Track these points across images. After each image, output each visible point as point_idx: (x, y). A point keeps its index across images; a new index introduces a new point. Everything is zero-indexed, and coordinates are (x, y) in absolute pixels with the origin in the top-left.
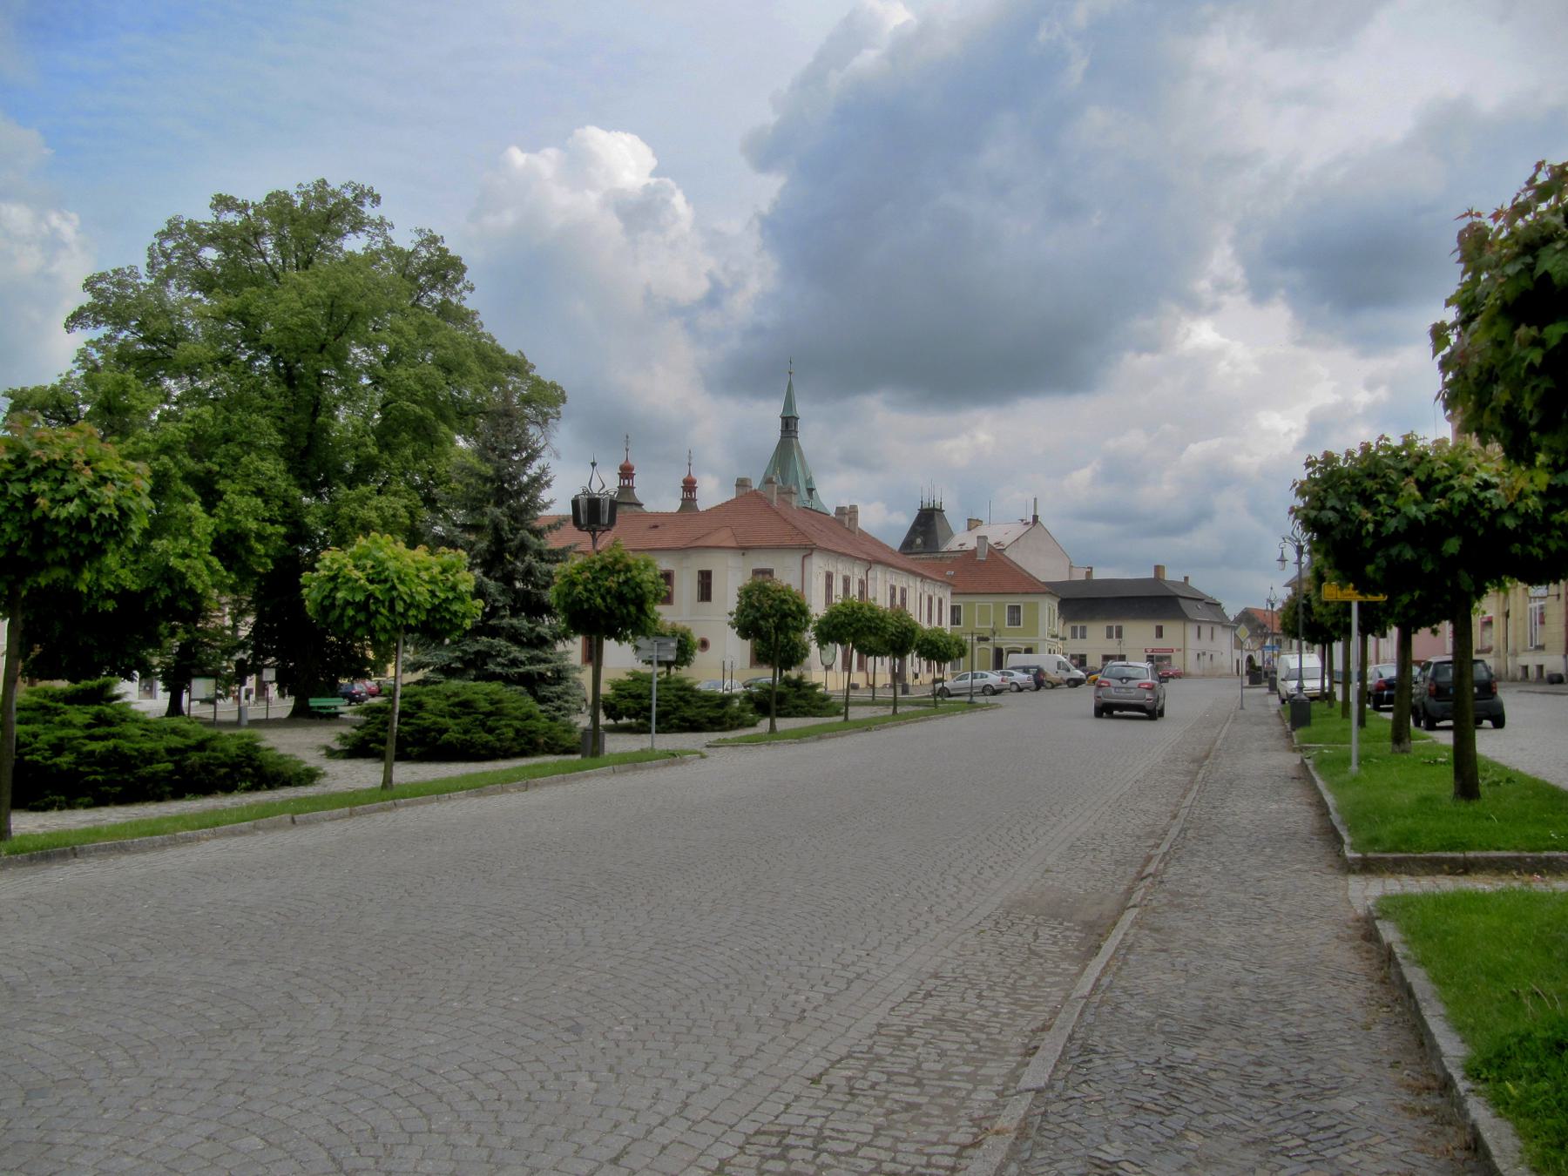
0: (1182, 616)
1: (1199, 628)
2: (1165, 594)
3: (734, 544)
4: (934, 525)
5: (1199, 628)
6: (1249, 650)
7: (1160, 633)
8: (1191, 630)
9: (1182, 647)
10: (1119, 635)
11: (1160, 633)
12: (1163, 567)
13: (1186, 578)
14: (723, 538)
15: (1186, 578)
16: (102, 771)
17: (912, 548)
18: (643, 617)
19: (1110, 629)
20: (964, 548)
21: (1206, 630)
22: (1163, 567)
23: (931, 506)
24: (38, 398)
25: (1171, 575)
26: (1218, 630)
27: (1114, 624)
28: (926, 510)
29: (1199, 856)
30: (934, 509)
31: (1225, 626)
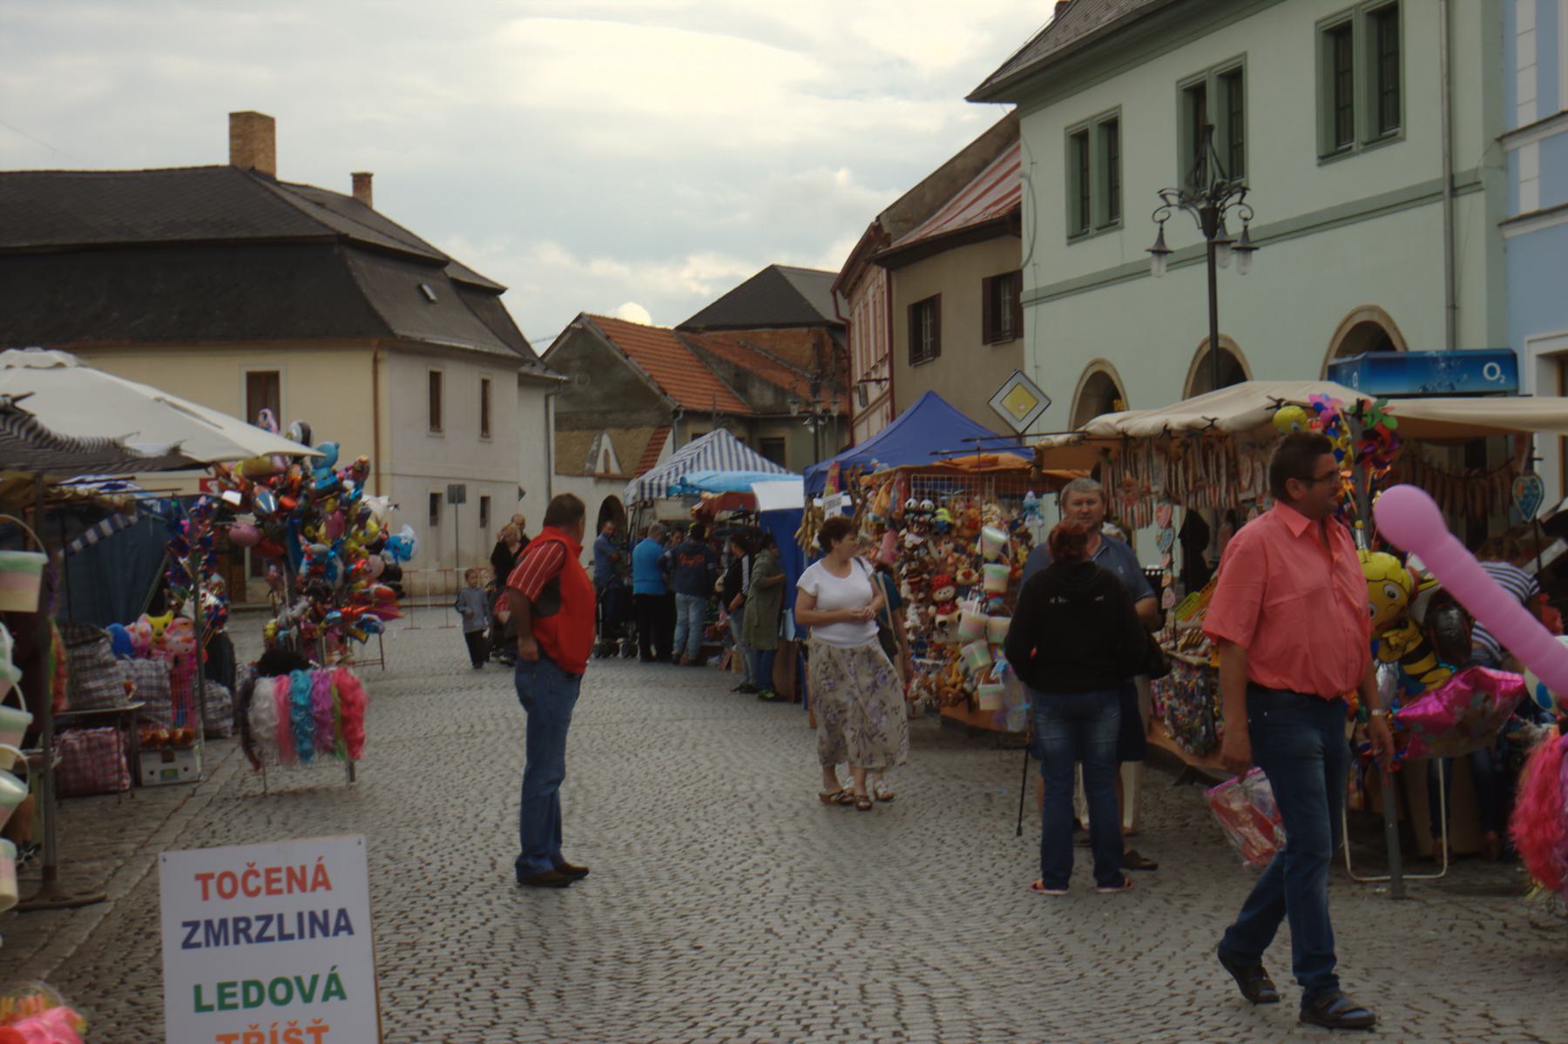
1: (435, 379)
5: (435, 379)
17: (557, 473)
22: (267, 123)
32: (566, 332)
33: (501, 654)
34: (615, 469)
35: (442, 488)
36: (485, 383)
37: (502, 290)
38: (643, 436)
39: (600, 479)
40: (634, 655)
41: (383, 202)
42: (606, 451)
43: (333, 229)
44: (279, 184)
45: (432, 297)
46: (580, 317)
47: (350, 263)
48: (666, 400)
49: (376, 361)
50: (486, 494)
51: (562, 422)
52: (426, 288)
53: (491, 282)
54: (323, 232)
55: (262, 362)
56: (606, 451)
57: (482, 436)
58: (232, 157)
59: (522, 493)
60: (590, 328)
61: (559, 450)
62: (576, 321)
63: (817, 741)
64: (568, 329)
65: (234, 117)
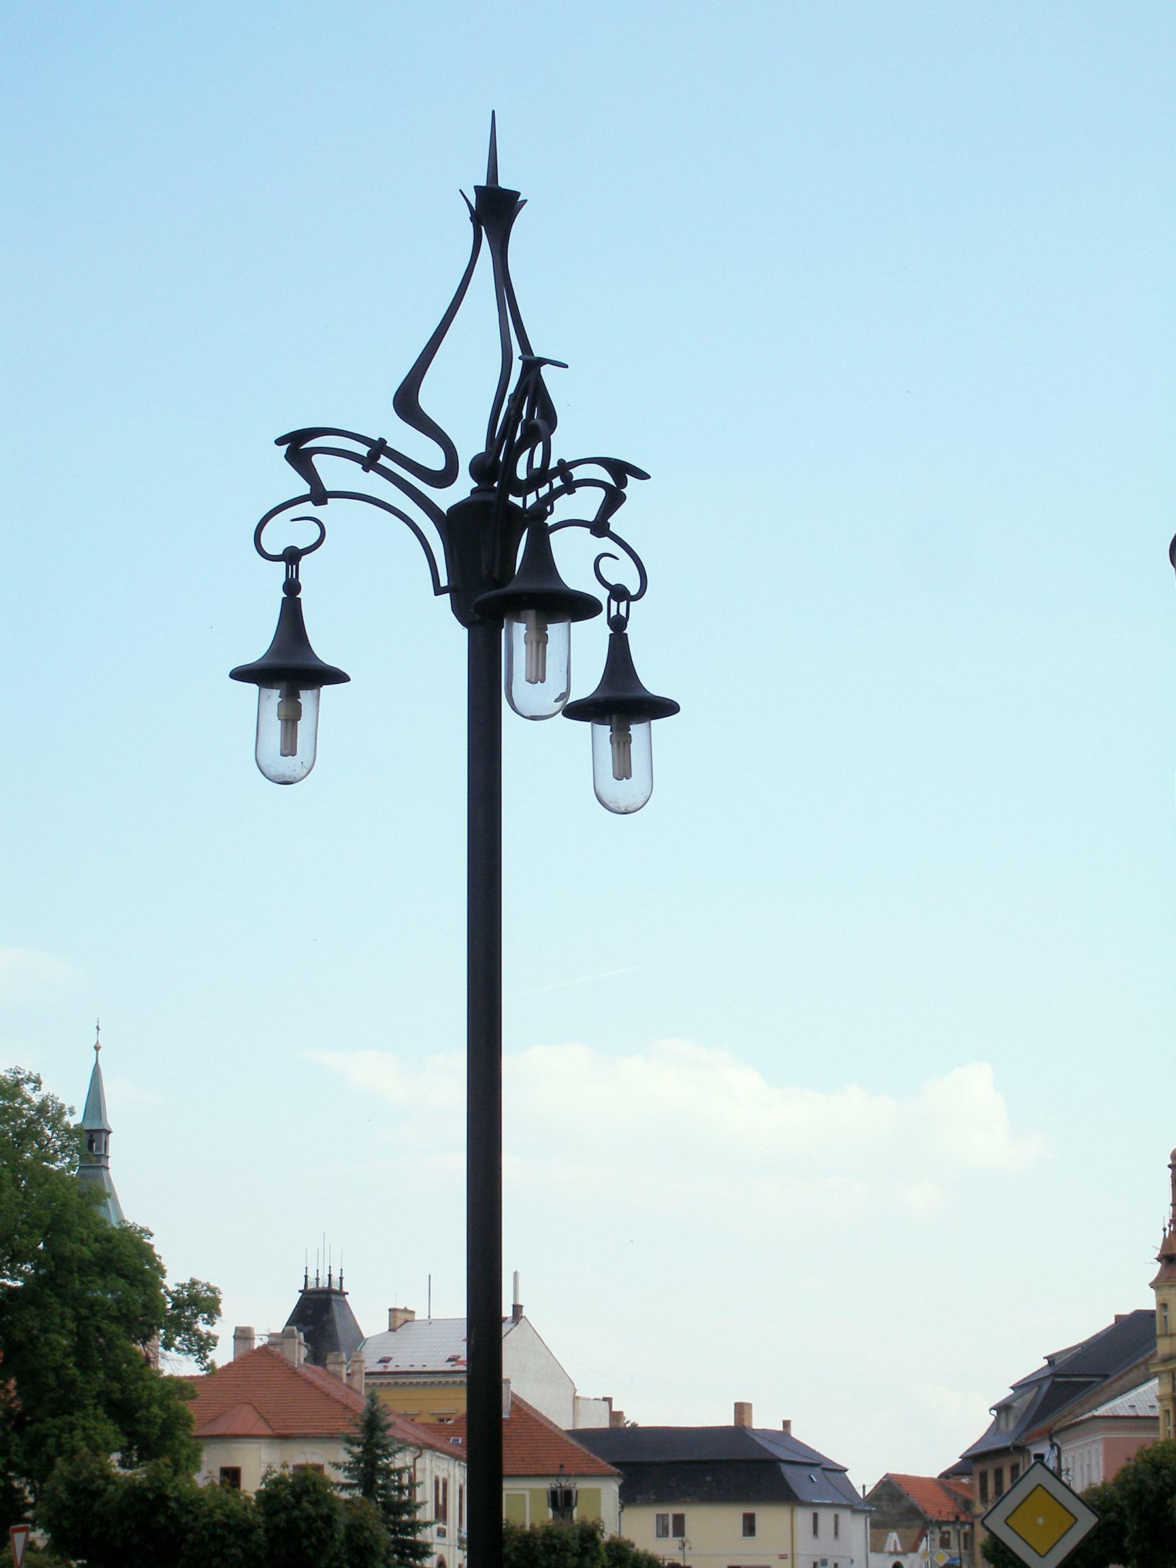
0: (784, 1495)
1: (815, 1516)
2: (758, 1457)
3: (269, 1432)
4: (332, 1321)
5: (815, 1516)
6: (896, 1553)
7: (749, 1527)
8: (803, 1517)
9: (788, 1552)
10: (679, 1530)
11: (749, 1527)
12: (749, 1406)
13: (786, 1424)
14: (244, 1419)
15: (786, 1424)
16: (1167, 1236)
17: (871, 1551)
18: (339, 1488)
19: (661, 1518)
20: (391, 1367)
21: (826, 1518)
22: (749, 1406)
23: (324, 1283)
24: (1092, 1536)
25: (763, 1420)
26: (846, 1517)
27: (671, 1511)
28: (313, 1292)
29: (513, 1425)
30: (329, 1291)
31: (855, 1511)
32: (879, 1483)
33: (27, 1217)
34: (899, 1549)
35: (818, 1560)
36: (836, 1516)
37: (846, 1470)
38: (916, 1532)
39: (891, 1553)
40: (350, 1528)
41: (795, 1433)
42: (895, 1541)
43: (776, 1456)
44: (753, 1430)
45: (815, 1480)
46: (887, 1475)
47: (782, 1469)
48: (925, 1515)
49: (792, 1509)
50: (836, 1562)
51: (874, 1525)
52: (812, 1476)
53: (841, 1466)
54: (772, 1457)
55: (749, 1509)
56: (895, 1541)
57: (835, 1538)
58: (735, 1423)
59: (852, 1561)
60: (891, 1481)
61: (872, 1536)
62: (884, 1478)
63: (343, 1451)
64: (881, 1481)
65: (436, 595)
